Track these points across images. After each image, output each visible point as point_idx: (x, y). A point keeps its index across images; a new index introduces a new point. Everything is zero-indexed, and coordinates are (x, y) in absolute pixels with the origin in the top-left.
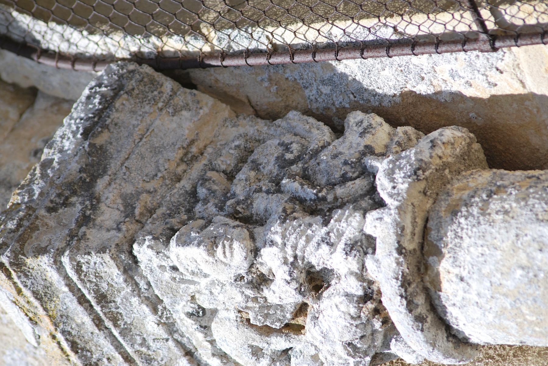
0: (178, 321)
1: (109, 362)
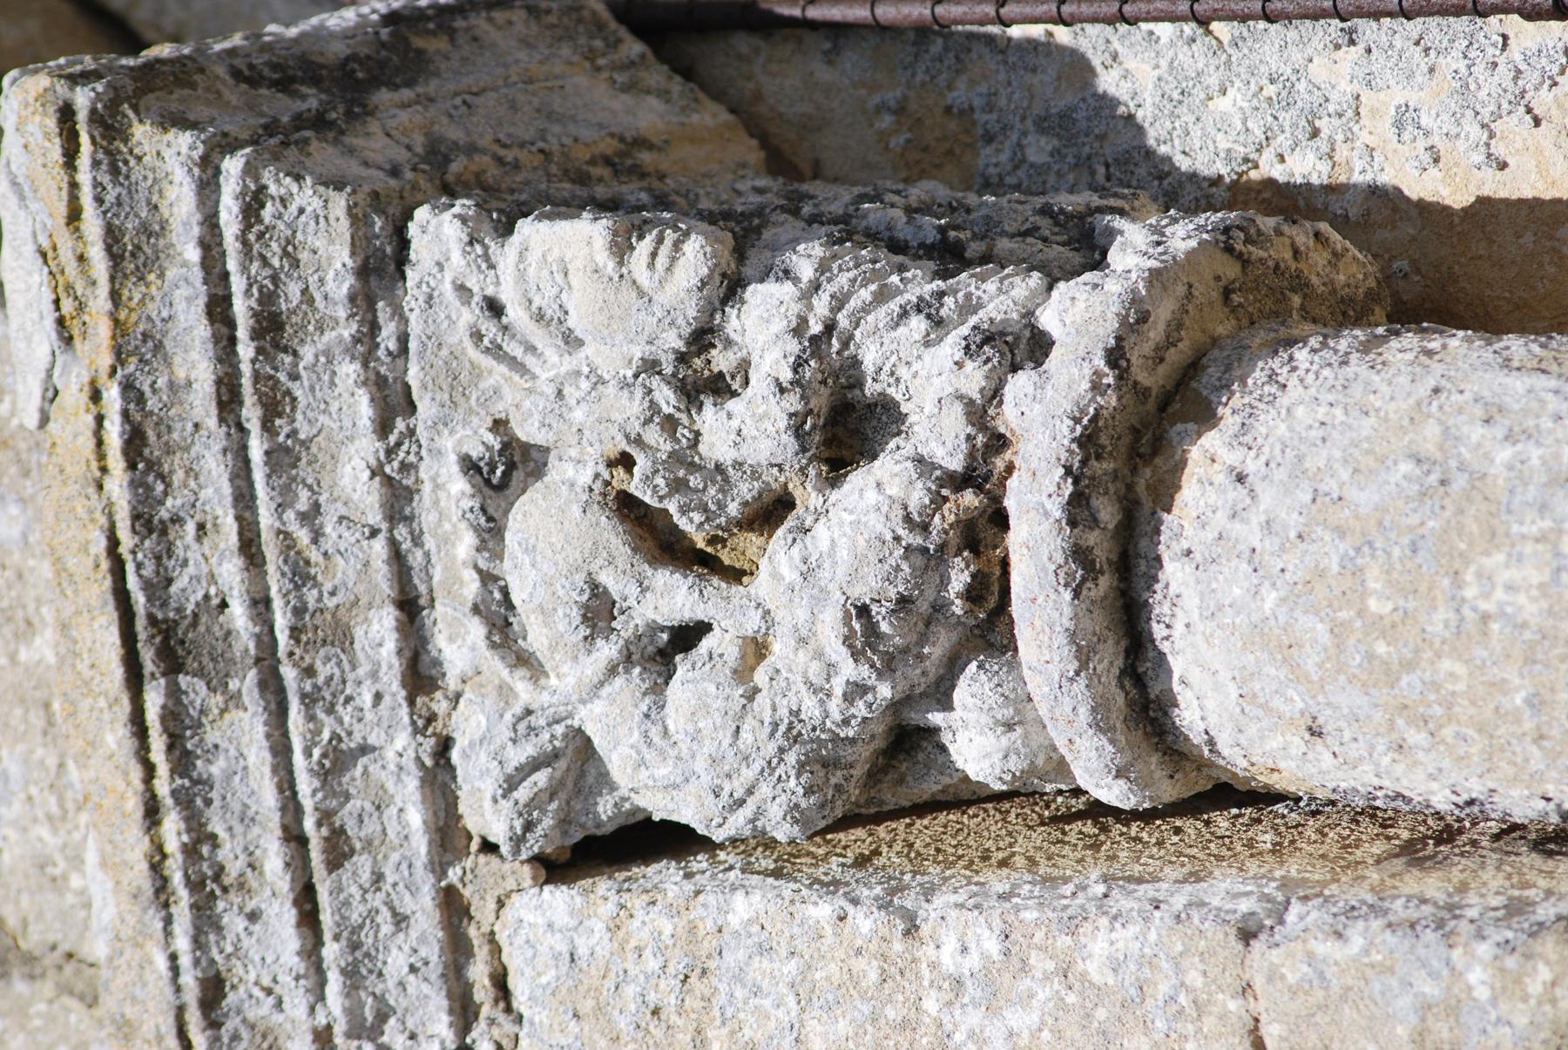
0: (427, 488)
1: (199, 539)
